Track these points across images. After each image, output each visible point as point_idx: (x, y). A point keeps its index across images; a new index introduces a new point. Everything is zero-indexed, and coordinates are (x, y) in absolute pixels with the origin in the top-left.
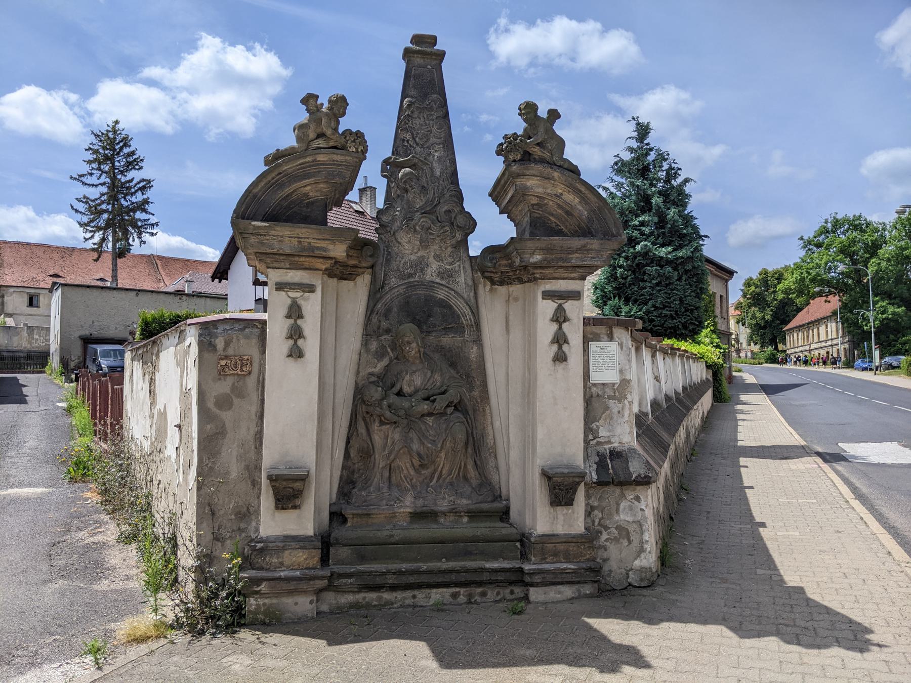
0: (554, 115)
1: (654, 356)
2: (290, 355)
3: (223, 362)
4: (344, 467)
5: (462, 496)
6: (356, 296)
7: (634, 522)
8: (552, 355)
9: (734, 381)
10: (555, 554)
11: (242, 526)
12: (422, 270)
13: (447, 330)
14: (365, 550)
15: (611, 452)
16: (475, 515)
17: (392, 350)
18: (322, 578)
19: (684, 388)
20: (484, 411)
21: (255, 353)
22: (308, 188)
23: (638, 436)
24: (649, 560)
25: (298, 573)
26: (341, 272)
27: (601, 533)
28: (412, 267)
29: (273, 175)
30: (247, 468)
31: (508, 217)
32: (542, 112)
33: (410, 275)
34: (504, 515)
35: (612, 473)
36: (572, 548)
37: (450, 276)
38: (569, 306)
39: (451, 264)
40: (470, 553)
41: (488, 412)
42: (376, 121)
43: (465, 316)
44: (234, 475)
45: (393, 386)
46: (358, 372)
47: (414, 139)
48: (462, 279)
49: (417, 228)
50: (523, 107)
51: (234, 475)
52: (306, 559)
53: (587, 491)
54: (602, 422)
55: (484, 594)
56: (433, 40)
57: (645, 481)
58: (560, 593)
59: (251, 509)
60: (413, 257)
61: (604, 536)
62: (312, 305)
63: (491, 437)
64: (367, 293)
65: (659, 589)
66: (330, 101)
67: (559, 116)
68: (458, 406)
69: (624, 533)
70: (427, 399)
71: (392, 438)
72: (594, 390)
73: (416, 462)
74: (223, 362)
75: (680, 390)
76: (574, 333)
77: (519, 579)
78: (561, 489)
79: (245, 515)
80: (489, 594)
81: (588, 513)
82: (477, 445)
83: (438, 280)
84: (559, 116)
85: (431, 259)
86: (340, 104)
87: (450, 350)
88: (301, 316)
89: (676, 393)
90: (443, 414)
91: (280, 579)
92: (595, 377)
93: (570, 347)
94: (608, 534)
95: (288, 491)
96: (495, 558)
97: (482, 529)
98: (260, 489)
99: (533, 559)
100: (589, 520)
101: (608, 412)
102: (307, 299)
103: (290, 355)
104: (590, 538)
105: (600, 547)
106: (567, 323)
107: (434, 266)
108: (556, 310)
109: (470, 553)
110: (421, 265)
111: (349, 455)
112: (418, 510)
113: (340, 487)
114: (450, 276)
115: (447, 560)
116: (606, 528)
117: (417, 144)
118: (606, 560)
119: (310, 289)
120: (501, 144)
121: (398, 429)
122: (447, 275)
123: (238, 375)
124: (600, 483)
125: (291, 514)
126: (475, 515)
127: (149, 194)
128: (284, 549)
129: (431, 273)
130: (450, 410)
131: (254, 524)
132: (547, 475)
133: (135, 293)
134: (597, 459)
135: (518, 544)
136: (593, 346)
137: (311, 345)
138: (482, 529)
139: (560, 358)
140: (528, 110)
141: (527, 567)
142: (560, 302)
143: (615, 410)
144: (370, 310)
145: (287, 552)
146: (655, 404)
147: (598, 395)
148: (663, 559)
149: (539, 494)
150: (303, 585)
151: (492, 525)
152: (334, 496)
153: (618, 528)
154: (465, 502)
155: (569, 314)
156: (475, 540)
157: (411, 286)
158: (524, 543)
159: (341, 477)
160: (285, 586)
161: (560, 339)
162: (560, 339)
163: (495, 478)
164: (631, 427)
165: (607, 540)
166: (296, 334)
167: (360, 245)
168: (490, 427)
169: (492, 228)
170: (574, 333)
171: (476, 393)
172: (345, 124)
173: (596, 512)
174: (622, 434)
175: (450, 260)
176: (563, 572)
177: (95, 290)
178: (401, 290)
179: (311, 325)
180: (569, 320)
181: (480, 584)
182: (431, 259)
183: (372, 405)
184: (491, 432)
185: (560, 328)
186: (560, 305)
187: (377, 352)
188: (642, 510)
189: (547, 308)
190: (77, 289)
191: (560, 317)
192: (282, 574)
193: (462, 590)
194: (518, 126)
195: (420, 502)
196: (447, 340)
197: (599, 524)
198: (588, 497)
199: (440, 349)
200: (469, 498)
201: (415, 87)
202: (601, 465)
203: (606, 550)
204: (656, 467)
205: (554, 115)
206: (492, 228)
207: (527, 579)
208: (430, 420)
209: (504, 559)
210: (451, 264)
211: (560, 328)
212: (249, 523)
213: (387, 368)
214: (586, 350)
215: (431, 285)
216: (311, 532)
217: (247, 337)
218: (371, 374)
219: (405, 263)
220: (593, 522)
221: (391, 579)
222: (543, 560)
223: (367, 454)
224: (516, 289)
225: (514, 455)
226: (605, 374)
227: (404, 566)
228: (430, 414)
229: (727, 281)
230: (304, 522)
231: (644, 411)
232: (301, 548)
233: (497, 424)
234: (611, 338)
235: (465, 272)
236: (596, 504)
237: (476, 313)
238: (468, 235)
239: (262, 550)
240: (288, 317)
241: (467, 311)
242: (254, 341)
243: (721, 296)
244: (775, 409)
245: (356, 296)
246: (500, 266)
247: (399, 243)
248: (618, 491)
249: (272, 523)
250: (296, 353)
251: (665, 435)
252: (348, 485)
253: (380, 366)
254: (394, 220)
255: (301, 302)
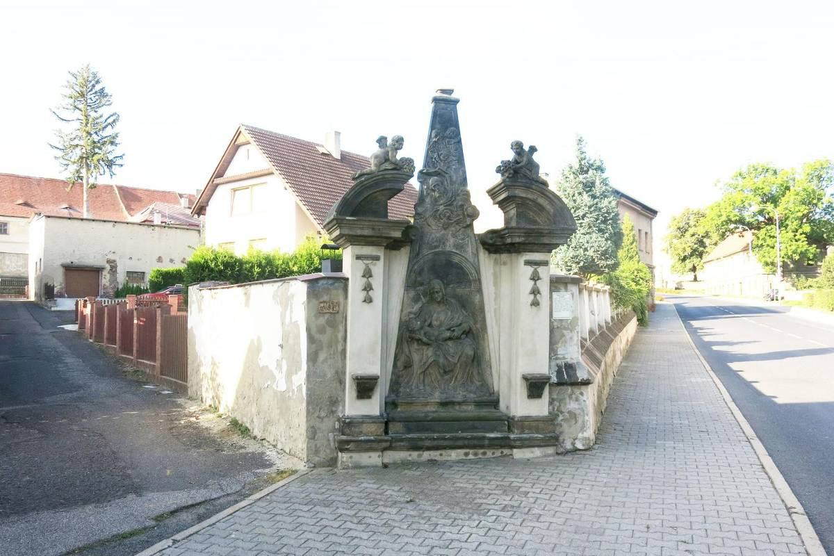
0: (533, 149)
1: (590, 295)
2: (365, 301)
3: (322, 305)
4: (393, 373)
5: (470, 392)
6: (401, 263)
7: (579, 409)
8: (530, 302)
9: (657, 308)
10: (530, 428)
11: (334, 409)
12: (444, 243)
13: (460, 283)
14: (414, 424)
15: (565, 364)
16: (479, 404)
17: (424, 296)
18: (386, 441)
19: (612, 318)
20: (484, 338)
21: (341, 299)
22: (378, 193)
23: (582, 354)
24: (590, 433)
25: (372, 438)
26: (393, 246)
27: (558, 415)
28: (436, 241)
29: (358, 187)
30: (337, 372)
31: (499, 207)
32: (526, 148)
33: (436, 247)
34: (495, 403)
35: (567, 379)
36: (541, 425)
37: (462, 247)
38: (541, 270)
39: (463, 239)
40: (476, 428)
41: (486, 337)
42: (415, 151)
43: (471, 274)
44: (329, 376)
45: (425, 321)
46: (402, 311)
47: (439, 157)
48: (469, 250)
49: (442, 217)
50: (514, 144)
51: (329, 376)
52: (376, 430)
53: (550, 389)
54: (560, 345)
55: (484, 454)
56: (450, 92)
57: (586, 383)
58: (532, 452)
59: (339, 399)
60: (438, 235)
61: (561, 418)
62: (378, 269)
63: (488, 354)
64: (407, 260)
65: (594, 452)
66: (393, 140)
67: (536, 150)
68: (468, 333)
69: (573, 416)
70: (449, 329)
71: (427, 355)
72: (555, 324)
73: (442, 371)
74: (322, 305)
75: (609, 320)
76: (544, 286)
77: (505, 443)
78: (535, 387)
79: (335, 402)
80: (488, 453)
81: (551, 403)
82: (478, 361)
83: (454, 250)
84: (536, 150)
85: (450, 236)
86: (399, 142)
87: (462, 296)
88: (371, 276)
89: (606, 322)
90: (458, 338)
91: (361, 441)
92: (556, 315)
93: (541, 297)
94: (563, 416)
95: (365, 387)
96: (492, 431)
97: (484, 412)
98: (345, 386)
99: (516, 431)
100: (551, 408)
101: (563, 339)
102: (375, 265)
103: (365, 301)
104: (551, 420)
105: (558, 425)
106: (540, 281)
107: (452, 240)
108: (533, 273)
109: (476, 428)
110: (442, 241)
111: (397, 367)
112: (444, 401)
113: (391, 386)
114: (462, 247)
115: (462, 432)
116: (562, 412)
117: (441, 161)
118: (561, 433)
119: (377, 258)
120: (500, 167)
121: (431, 349)
122: (460, 247)
123: (331, 313)
124: (560, 384)
125: (366, 402)
126: (479, 404)
127: (118, 128)
128: (363, 423)
129: (449, 246)
130: (463, 336)
131: (341, 408)
132: (525, 378)
133: (112, 224)
134: (557, 368)
135: (506, 422)
136: (555, 295)
137: (377, 294)
138: (484, 412)
139: (535, 304)
140: (518, 147)
141: (512, 436)
142: (535, 267)
143: (568, 337)
144: (410, 271)
145: (364, 425)
146: (591, 332)
147: (558, 327)
148: (600, 431)
149: (520, 389)
150: (375, 445)
151: (490, 410)
152: (387, 392)
153: (569, 412)
154: (472, 395)
155: (541, 276)
156: (480, 419)
157: (437, 254)
158: (510, 422)
159: (391, 380)
160: (364, 445)
161: (535, 292)
162: (535, 292)
163: (489, 381)
164: (578, 348)
165: (562, 420)
166: (368, 288)
167: (407, 229)
168: (487, 349)
169: (490, 218)
170: (544, 286)
171: (478, 326)
172: (400, 155)
173: (555, 402)
174: (571, 352)
175: (462, 237)
176: (535, 439)
177: (75, 221)
178: (430, 256)
179: (377, 282)
180: (540, 279)
181: (482, 447)
182: (450, 236)
183: (409, 335)
184: (488, 352)
185: (535, 284)
186: (536, 269)
187: (414, 298)
188: (584, 401)
189: (529, 270)
190: (61, 220)
191: (535, 278)
192: (362, 438)
193: (471, 451)
194: (510, 156)
195: (444, 396)
196: (460, 291)
197: (557, 410)
198: (550, 393)
199: (455, 296)
200: (475, 393)
201: (439, 123)
202: (559, 372)
203: (561, 426)
204: (594, 374)
205: (533, 149)
206: (490, 218)
207: (513, 443)
208: (450, 343)
209: (498, 431)
210: (463, 239)
211: (535, 284)
212: (337, 407)
213: (421, 309)
214: (551, 297)
215: (450, 253)
216: (378, 413)
217: (336, 289)
218: (410, 313)
219: (433, 239)
220: (554, 408)
221: (428, 443)
222: (523, 432)
223: (408, 366)
224: (504, 257)
225: (504, 367)
226: (561, 314)
227: (435, 436)
228: (450, 339)
229: (651, 219)
230: (373, 407)
231: (584, 337)
232: (373, 422)
233: (491, 346)
234: (566, 289)
235: (472, 245)
236: (555, 397)
237: (478, 272)
238: (473, 220)
239: (350, 423)
240: (364, 276)
241: (473, 271)
242: (341, 292)
243: (646, 233)
244: (686, 332)
245: (401, 263)
246: (496, 244)
247: (429, 225)
248: (570, 388)
249: (353, 407)
250: (368, 300)
251: (598, 355)
252: (395, 385)
253: (416, 308)
254: (426, 210)
255: (371, 267)
